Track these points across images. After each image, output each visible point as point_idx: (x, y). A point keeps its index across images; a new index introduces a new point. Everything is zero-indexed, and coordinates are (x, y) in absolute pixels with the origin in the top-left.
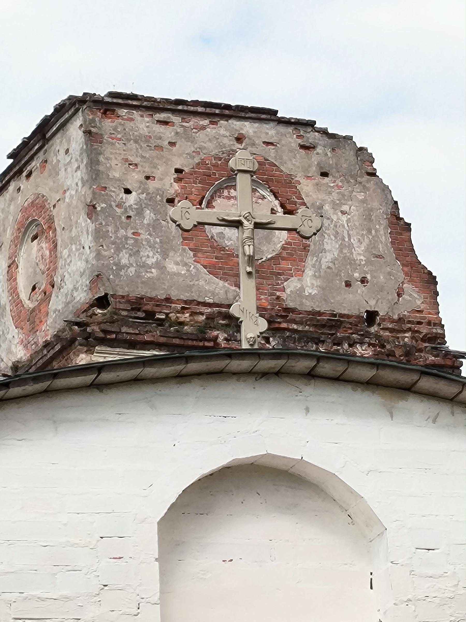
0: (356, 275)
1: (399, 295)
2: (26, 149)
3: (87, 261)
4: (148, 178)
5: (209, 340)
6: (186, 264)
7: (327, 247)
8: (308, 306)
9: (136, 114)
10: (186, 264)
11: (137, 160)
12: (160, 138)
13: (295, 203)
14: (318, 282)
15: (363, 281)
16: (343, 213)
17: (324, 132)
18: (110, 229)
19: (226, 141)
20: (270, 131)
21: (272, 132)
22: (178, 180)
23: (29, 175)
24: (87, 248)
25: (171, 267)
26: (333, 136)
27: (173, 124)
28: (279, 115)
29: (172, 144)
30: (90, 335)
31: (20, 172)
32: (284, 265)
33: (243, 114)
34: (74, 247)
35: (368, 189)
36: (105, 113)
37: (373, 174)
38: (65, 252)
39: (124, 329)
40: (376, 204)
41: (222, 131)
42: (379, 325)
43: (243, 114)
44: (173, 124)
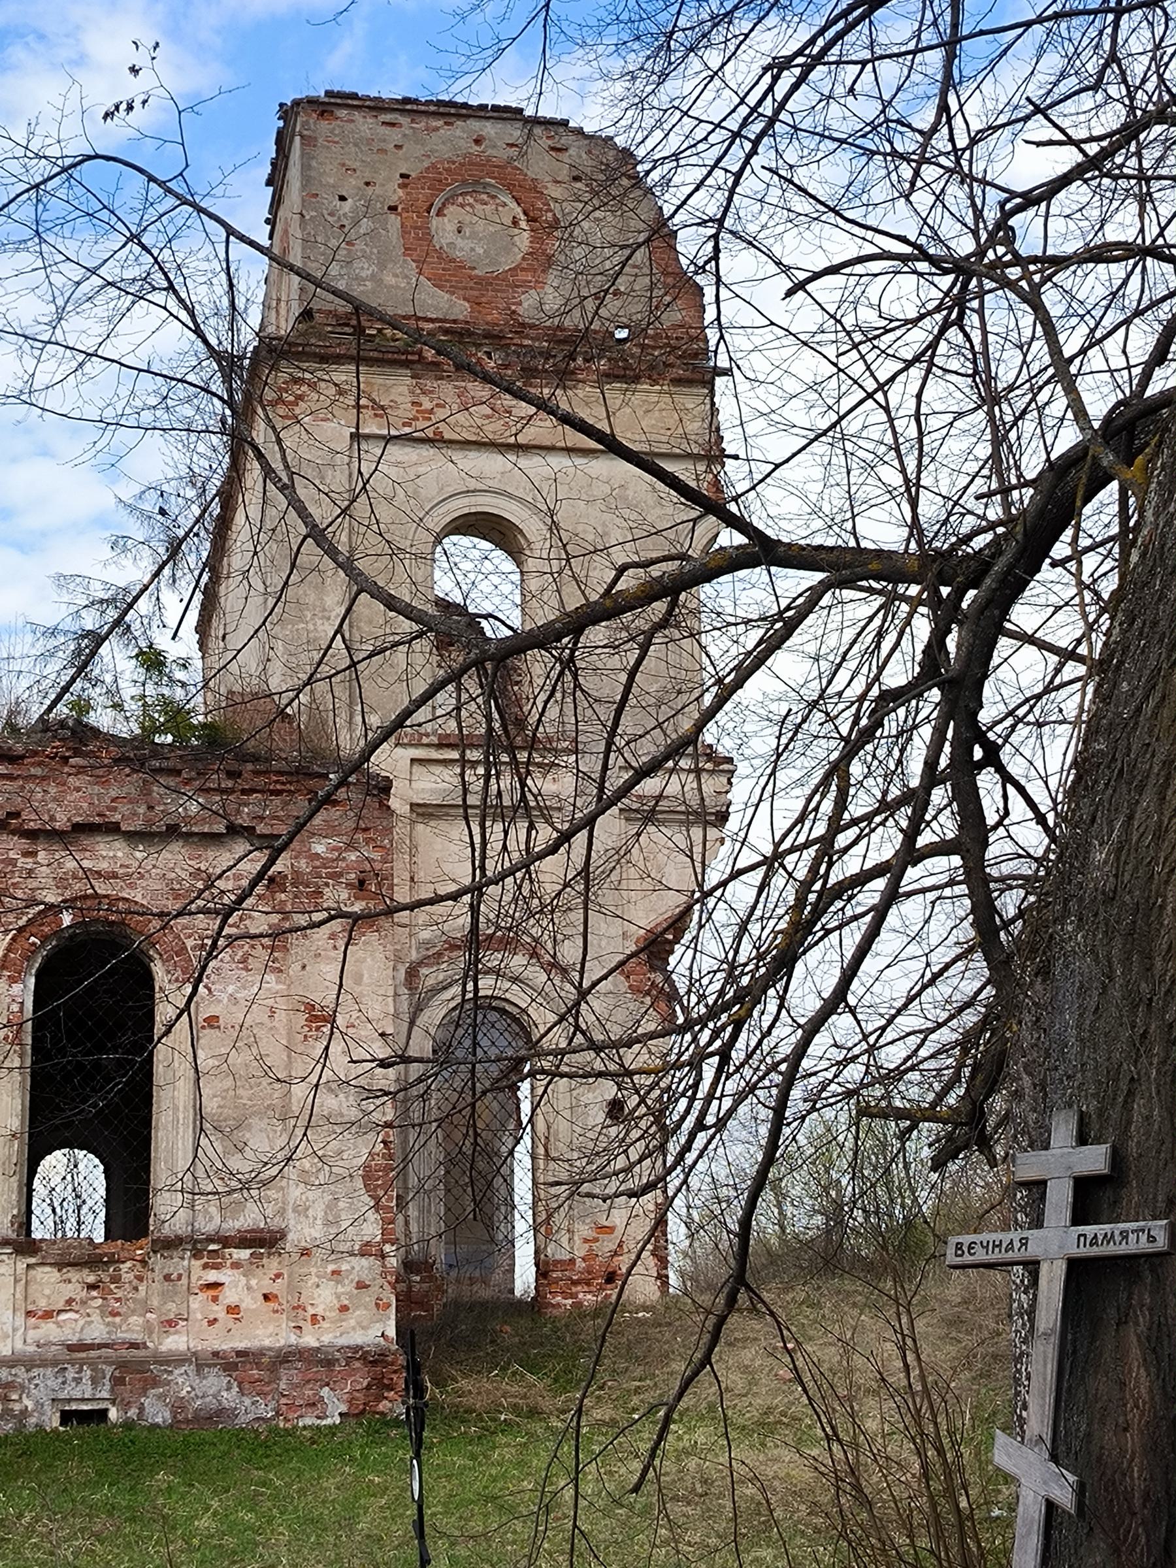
4: (367, 184)
9: (357, 115)
17: (579, 132)
22: (403, 186)
27: (401, 126)
44: (401, 126)
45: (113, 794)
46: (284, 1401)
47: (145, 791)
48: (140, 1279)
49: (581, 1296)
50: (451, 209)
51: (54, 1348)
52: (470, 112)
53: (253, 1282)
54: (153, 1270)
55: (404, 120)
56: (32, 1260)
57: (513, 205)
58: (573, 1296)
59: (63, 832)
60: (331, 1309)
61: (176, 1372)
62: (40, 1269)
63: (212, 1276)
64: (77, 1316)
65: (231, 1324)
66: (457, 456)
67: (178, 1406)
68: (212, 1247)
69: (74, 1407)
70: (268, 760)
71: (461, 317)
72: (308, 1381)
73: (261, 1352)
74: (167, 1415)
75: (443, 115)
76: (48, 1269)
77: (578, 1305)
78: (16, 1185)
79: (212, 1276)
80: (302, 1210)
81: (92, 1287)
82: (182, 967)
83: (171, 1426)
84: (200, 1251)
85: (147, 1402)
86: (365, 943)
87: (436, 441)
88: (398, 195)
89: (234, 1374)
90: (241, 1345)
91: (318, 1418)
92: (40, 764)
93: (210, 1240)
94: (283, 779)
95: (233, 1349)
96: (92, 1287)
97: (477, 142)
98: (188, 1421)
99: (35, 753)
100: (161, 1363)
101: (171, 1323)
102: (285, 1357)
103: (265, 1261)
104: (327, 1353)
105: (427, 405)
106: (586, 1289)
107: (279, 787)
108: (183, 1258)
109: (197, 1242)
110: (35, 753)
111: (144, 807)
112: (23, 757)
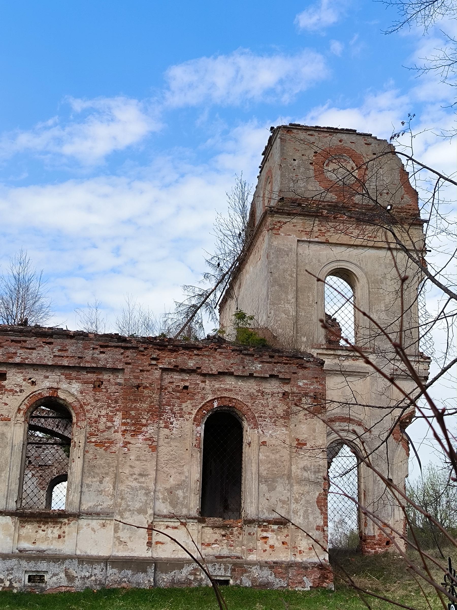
4: (303, 155)
9: (300, 132)
17: (375, 138)
20: (353, 138)
27: (314, 135)
28: (357, 132)
45: (232, 362)
46: (290, 581)
47: (242, 361)
48: (240, 534)
49: (377, 549)
51: (211, 557)
52: (338, 131)
53: (279, 537)
54: (244, 531)
55: (316, 134)
56: (204, 525)
57: (351, 162)
58: (375, 549)
59: (216, 375)
60: (306, 549)
61: (253, 568)
62: (206, 528)
63: (265, 534)
64: (219, 546)
65: (271, 552)
67: (254, 580)
68: (265, 524)
69: (218, 578)
70: (282, 352)
72: (299, 574)
73: (282, 563)
74: (250, 583)
75: (328, 132)
76: (209, 528)
77: (376, 552)
78: (198, 498)
79: (265, 534)
80: (296, 512)
81: (224, 536)
82: (254, 423)
83: (251, 587)
84: (260, 525)
85: (243, 578)
87: (327, 243)
89: (273, 570)
90: (275, 560)
91: (303, 588)
92: (207, 351)
93: (264, 521)
94: (288, 359)
95: (272, 561)
96: (224, 536)
98: (257, 586)
99: (206, 347)
100: (248, 564)
101: (250, 550)
102: (290, 565)
103: (283, 530)
104: (305, 564)
106: (379, 547)
107: (287, 362)
108: (255, 527)
109: (260, 521)
110: (206, 347)
111: (242, 367)
112: (202, 348)
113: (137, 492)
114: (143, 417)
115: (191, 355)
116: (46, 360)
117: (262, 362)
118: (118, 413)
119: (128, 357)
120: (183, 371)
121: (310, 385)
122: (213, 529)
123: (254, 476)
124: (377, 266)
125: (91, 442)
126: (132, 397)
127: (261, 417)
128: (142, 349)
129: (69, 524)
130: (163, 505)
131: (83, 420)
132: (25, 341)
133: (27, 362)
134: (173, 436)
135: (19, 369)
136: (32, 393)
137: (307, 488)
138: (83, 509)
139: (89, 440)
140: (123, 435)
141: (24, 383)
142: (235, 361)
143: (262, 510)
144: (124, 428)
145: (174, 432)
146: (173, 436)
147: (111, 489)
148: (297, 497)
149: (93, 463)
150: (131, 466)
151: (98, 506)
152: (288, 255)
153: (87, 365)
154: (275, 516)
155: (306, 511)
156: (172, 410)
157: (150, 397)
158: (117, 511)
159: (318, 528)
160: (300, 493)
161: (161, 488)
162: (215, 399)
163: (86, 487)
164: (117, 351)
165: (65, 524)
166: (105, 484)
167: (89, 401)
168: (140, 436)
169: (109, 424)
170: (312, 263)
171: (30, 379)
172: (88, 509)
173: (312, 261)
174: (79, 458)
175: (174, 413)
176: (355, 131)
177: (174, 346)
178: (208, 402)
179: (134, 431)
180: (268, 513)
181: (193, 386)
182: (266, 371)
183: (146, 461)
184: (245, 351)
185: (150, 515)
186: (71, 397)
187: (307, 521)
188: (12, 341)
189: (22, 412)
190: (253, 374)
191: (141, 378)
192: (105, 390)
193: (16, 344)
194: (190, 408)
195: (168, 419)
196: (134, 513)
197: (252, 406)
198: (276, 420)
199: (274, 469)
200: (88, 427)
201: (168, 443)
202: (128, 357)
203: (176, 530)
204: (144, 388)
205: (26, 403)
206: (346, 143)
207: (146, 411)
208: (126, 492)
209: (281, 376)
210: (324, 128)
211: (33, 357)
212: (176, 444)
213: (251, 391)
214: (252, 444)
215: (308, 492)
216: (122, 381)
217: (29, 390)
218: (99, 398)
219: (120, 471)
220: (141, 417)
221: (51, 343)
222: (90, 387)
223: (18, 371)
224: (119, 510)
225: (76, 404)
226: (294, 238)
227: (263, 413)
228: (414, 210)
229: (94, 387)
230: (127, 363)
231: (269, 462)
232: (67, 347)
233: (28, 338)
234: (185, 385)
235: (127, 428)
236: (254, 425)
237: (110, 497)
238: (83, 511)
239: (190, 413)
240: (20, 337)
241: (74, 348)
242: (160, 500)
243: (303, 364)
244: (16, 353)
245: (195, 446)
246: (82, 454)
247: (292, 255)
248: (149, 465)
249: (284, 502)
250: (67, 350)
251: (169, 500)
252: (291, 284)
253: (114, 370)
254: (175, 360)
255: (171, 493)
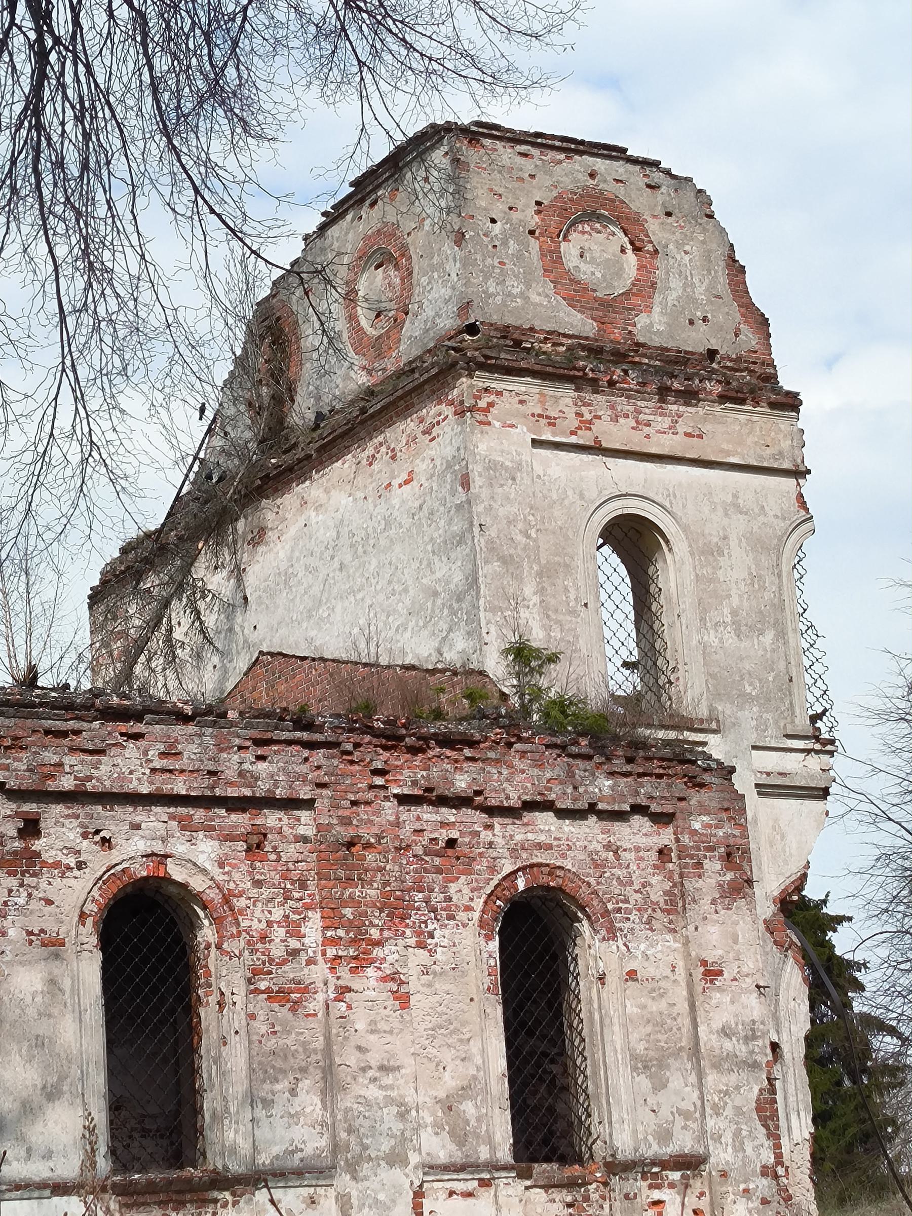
0: (699, 314)
1: (737, 335)
2: (373, 178)
3: (454, 288)
4: (511, 208)
5: (579, 370)
6: (547, 296)
7: (672, 285)
8: (656, 341)
9: (499, 145)
10: (547, 296)
11: (501, 190)
12: (521, 170)
13: (643, 241)
14: (664, 319)
15: (705, 319)
16: (686, 253)
17: (668, 173)
18: (478, 257)
19: (580, 176)
20: (620, 168)
21: (621, 170)
22: (538, 212)
23: (372, 205)
24: (453, 275)
25: (535, 298)
26: (675, 177)
27: (532, 157)
28: (628, 153)
29: (532, 176)
30: (471, 360)
31: (362, 201)
32: (635, 301)
33: (596, 151)
34: (436, 275)
35: (708, 230)
36: (470, 142)
37: (711, 216)
38: (424, 280)
39: (503, 356)
40: (714, 246)
41: (577, 167)
42: (719, 363)
43: (596, 151)
44: (532, 157)
45: (548, 776)
47: (570, 774)
48: (603, 1198)
50: (573, 236)
56: (528, 1183)
63: (656, 1195)
66: (610, 461)
68: (655, 1170)
71: (591, 335)
76: (538, 1190)
79: (656, 1195)
80: (718, 1138)
81: (569, 1205)
86: (737, 908)
88: (534, 221)
93: (654, 1164)
97: (592, 175)
105: (587, 416)
107: (662, 771)
108: (636, 1180)
112: (478, 742)
113: (379, 1113)
114: (371, 922)
115: (456, 761)
116: (135, 783)
117: (611, 774)
118: (310, 914)
119: (319, 767)
120: (443, 801)
121: (717, 827)
122: (546, 1192)
123: (620, 1057)
124: (706, 509)
125: (257, 991)
126: (342, 873)
127: (619, 910)
128: (349, 747)
129: (235, 1203)
130: (435, 1139)
131: (232, 936)
132: (77, 733)
133: (89, 786)
134: (437, 968)
135: (69, 808)
136: (108, 871)
137: (733, 1078)
138: (261, 1162)
139: (252, 987)
140: (332, 969)
141: (86, 843)
142: (556, 772)
143: (646, 1138)
144: (331, 952)
145: (438, 956)
146: (437, 968)
147: (317, 1109)
148: (717, 1099)
149: (269, 1044)
150: (359, 1048)
151: (293, 1152)
152: (514, 479)
153: (232, 792)
154: (671, 1149)
155: (737, 1134)
156: (427, 901)
157: (381, 869)
158: (342, 1163)
159: (765, 1171)
160: (720, 1092)
161: (427, 1099)
162: (519, 870)
163: (260, 1106)
164: (294, 753)
165: (225, 1206)
166: (302, 1096)
167: (242, 885)
168: (370, 972)
169: (294, 944)
170: (566, 502)
171: (97, 832)
172: (272, 1162)
173: (567, 496)
174: (237, 1032)
175: (434, 910)
176: (624, 150)
177: (419, 739)
178: (504, 878)
179: (356, 958)
180: (658, 1144)
181: (467, 840)
182: (622, 798)
183: (391, 1032)
184: (573, 748)
185: (416, 1168)
186: (201, 877)
187: (740, 1155)
188: (47, 732)
189: (89, 921)
190: (595, 804)
191: (355, 822)
192: (273, 857)
193: (58, 741)
194: (470, 895)
195: (423, 926)
196: (379, 1165)
197: (598, 883)
198: (651, 918)
199: (659, 1036)
200: (246, 952)
201: (430, 985)
202: (319, 767)
203: (470, 1200)
204: (364, 848)
205: (97, 896)
206: (605, 181)
207: (375, 906)
208: (356, 1114)
209: (654, 808)
210: (553, 137)
211: (106, 773)
212: (447, 987)
213: (591, 848)
214: (608, 979)
215: (737, 1088)
216: (310, 832)
217: (99, 862)
218: (263, 877)
219: (338, 1060)
220: (367, 923)
221: (137, 736)
222: (239, 848)
223: (67, 812)
224: (347, 1160)
225: (213, 895)
226: (523, 434)
227: (622, 902)
228: (763, 364)
229: (249, 850)
230: (321, 785)
231: (649, 1022)
232: (179, 746)
233: (85, 724)
234: (451, 836)
235: (340, 953)
236: (608, 933)
237: (318, 1128)
238: (261, 1167)
239: (469, 909)
240: (66, 720)
241: (193, 748)
242: (429, 1129)
243: (695, 777)
244: (60, 765)
245: (489, 988)
246: (244, 1023)
247: (522, 479)
248: (398, 1043)
249: (686, 1115)
250: (180, 753)
251: (447, 1128)
252: (529, 558)
253: (291, 804)
254: (424, 773)
255: (450, 1108)
